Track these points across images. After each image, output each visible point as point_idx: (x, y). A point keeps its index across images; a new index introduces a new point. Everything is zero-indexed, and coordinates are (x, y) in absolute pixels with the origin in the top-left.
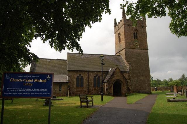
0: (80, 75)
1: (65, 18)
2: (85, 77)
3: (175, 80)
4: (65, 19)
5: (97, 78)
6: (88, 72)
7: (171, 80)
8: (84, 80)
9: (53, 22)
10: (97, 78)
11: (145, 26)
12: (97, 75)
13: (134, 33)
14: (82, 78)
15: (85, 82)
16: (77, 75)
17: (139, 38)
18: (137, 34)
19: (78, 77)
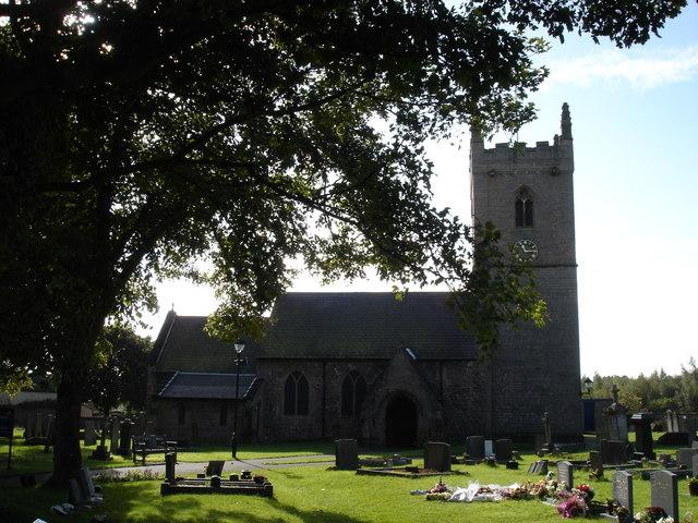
0: (297, 374)
1: (189, 136)
2: (313, 382)
3: (636, 377)
4: (191, 138)
5: (297, 382)
6: (324, 361)
7: (624, 380)
8: (311, 390)
9: (44, 367)
10: (297, 382)
11: (561, 167)
12: (355, 373)
13: (519, 203)
14: (304, 385)
15: (313, 395)
16: (288, 375)
17: (537, 220)
18: (529, 203)
19: (290, 380)
